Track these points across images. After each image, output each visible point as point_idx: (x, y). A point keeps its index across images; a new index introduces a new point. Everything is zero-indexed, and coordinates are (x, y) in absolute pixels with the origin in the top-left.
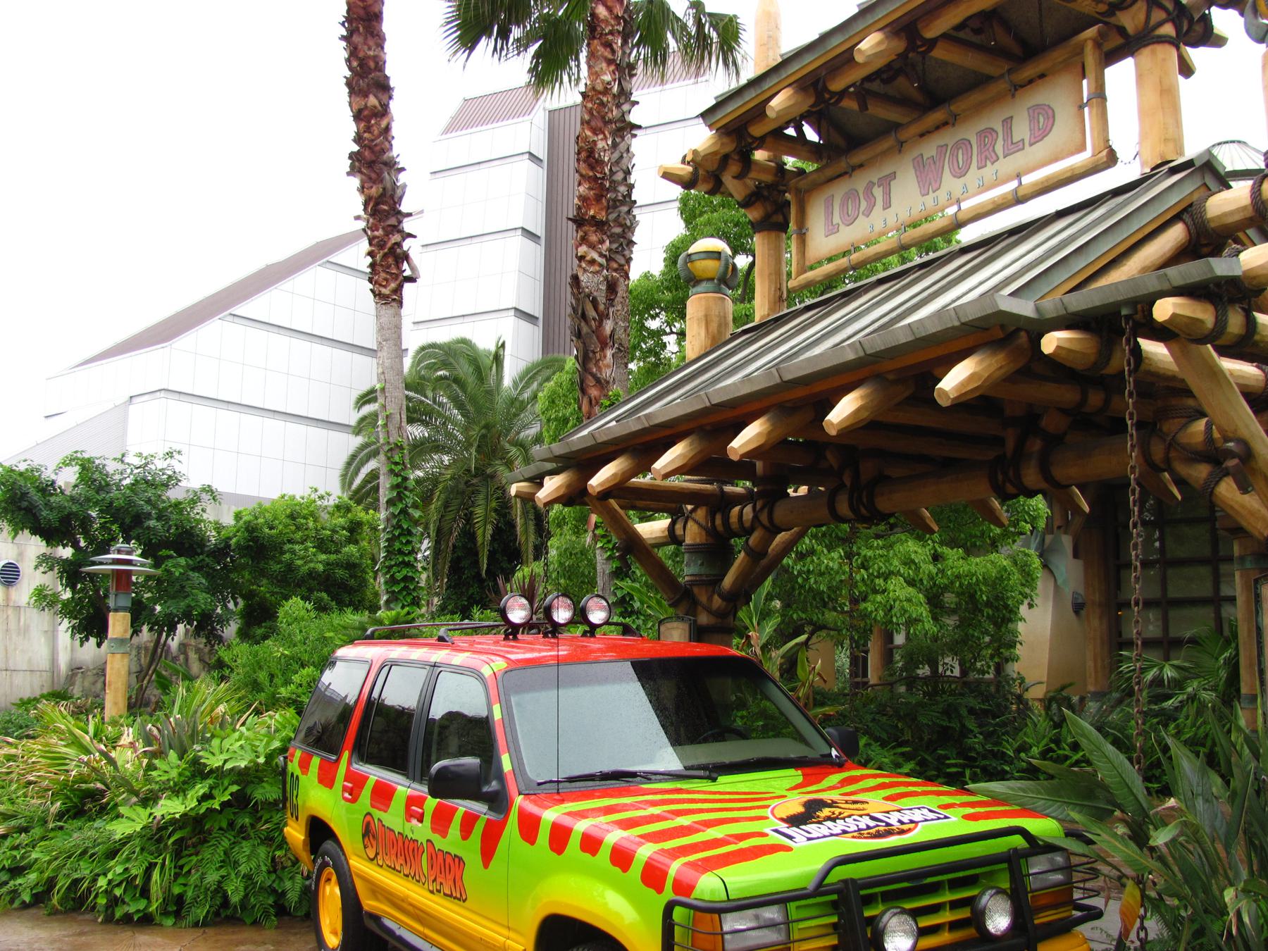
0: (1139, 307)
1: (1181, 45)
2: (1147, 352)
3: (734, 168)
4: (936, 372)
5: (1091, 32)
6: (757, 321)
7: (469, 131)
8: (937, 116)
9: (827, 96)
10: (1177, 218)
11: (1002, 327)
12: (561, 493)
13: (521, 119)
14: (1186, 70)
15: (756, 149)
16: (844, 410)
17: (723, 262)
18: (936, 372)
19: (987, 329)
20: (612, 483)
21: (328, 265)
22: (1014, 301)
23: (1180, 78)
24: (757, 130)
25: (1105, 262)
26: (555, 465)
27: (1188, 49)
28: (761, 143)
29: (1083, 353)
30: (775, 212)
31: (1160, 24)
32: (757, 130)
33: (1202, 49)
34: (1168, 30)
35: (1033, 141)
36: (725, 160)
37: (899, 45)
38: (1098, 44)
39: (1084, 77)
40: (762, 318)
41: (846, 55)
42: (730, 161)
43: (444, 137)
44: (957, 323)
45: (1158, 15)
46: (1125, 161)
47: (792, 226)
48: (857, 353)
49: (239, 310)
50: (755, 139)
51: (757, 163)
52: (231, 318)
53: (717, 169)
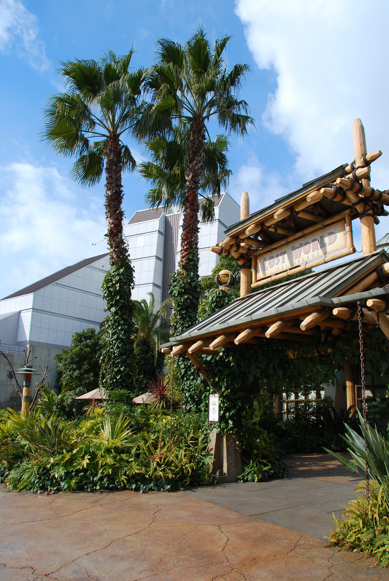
0: (363, 301)
1: (375, 215)
2: (365, 314)
3: (234, 249)
4: (301, 318)
5: (348, 211)
6: (241, 297)
7: (138, 223)
8: (299, 234)
9: (265, 227)
10: (374, 270)
11: (321, 306)
12: (179, 352)
13: (156, 219)
14: (377, 222)
15: (242, 242)
16: (272, 328)
17: (230, 277)
18: (301, 318)
19: (316, 306)
20: (196, 350)
21: (89, 267)
22: (324, 298)
23: (375, 224)
24: (242, 237)
25: (352, 285)
26: (176, 343)
27: (378, 216)
28: (243, 241)
29: (311, 221)
30: (247, 262)
31: (368, 210)
32: (242, 237)
33: (381, 216)
34: (370, 212)
35: (330, 244)
36: (231, 246)
37: (288, 214)
38: (349, 215)
39: (345, 223)
40: (243, 296)
41: (271, 216)
42: (233, 246)
43: (128, 225)
44: (307, 305)
45: (368, 207)
46: (359, 251)
47: (253, 266)
48: (276, 312)
49: (58, 282)
50: (241, 240)
51: (242, 247)
52: (56, 285)
53: (229, 249)
